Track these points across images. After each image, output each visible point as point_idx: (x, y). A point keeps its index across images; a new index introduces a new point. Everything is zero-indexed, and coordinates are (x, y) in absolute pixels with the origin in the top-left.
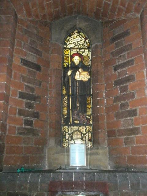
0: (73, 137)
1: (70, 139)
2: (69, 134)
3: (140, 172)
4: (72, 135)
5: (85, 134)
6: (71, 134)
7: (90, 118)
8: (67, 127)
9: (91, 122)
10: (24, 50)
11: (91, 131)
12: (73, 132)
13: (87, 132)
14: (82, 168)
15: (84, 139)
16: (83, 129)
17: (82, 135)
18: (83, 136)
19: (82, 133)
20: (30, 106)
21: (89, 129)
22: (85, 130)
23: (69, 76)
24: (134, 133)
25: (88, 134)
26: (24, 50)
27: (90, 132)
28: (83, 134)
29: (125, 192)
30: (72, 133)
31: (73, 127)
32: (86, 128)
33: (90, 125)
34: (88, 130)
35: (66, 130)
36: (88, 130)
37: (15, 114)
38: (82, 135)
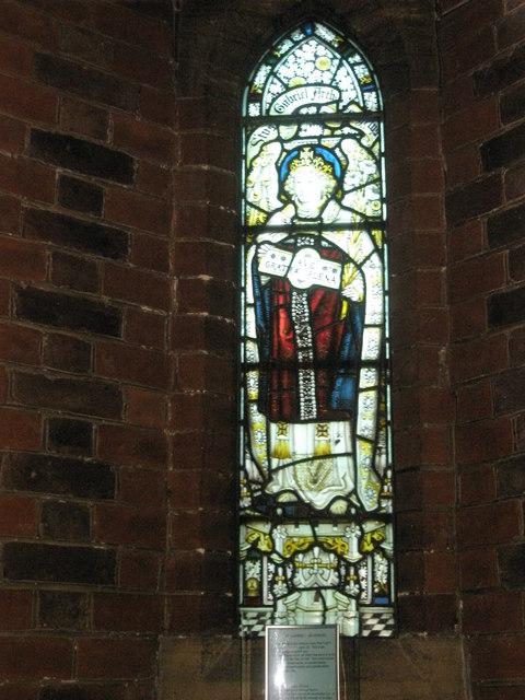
1: (280, 588)
3: (365, 284)
5: (357, 566)
8: (266, 528)
10: (206, 314)
11: (388, 547)
12: (296, 553)
13: (365, 554)
15: (353, 588)
18: (348, 574)
19: (340, 557)
21: (375, 536)
22: (355, 542)
23: (320, 233)
25: (373, 564)
26: (206, 314)
27: (384, 555)
28: (345, 560)
31: (297, 526)
32: (362, 530)
34: (373, 540)
35: (259, 539)
36: (373, 540)
37: (102, 428)
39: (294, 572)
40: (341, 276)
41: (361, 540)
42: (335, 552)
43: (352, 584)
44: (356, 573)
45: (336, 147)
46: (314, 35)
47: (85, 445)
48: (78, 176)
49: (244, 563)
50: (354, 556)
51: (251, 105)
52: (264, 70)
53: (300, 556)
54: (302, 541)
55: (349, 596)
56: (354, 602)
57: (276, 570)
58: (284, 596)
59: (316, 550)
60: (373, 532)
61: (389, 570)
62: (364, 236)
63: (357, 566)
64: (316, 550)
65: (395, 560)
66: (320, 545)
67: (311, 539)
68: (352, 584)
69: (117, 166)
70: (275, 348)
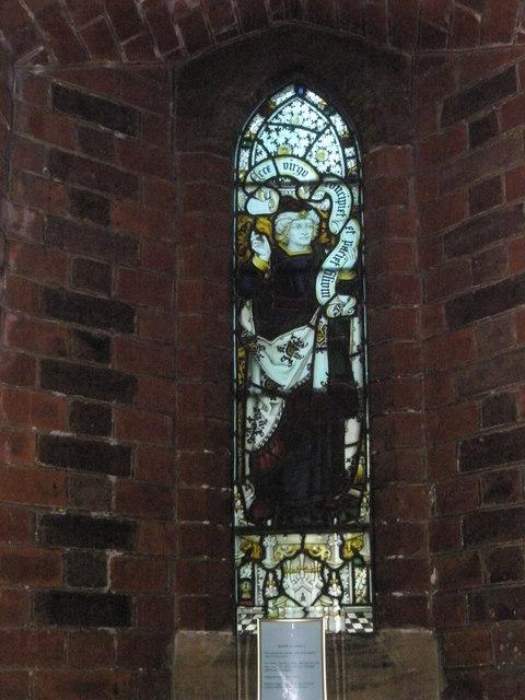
0: (282, 581)
1: (271, 591)
2: (341, 605)
4: (279, 573)
6: (273, 571)
7: (362, 495)
9: (365, 513)
11: (366, 553)
12: (285, 559)
13: (346, 561)
14: (348, 418)
16: (327, 545)
17: (326, 571)
18: (330, 577)
19: (324, 564)
20: (100, 348)
24: (57, 596)
29: (63, 14)
30: (281, 565)
32: (342, 539)
33: (362, 528)
38: (326, 571)
39: (283, 576)
40: (294, 601)
41: (342, 547)
42: (318, 559)
43: (335, 585)
44: (338, 577)
45: (276, 567)
46: (303, 97)
47: (105, 285)
48: (87, 401)
49: (257, 398)
50: (337, 561)
51: (258, 115)
52: (259, 120)
53: (288, 562)
54: (290, 548)
55: (332, 598)
56: (336, 602)
57: (267, 574)
58: (275, 598)
59: (302, 556)
60: (352, 540)
61: (368, 575)
62: (345, 190)
63: (337, 571)
64: (302, 556)
65: (374, 566)
66: (307, 553)
67: (298, 547)
68: (335, 585)
69: (122, 316)
70: (239, 657)
